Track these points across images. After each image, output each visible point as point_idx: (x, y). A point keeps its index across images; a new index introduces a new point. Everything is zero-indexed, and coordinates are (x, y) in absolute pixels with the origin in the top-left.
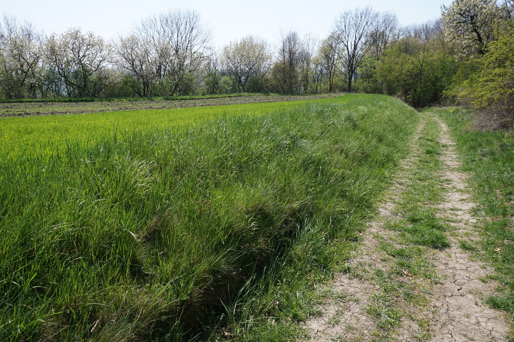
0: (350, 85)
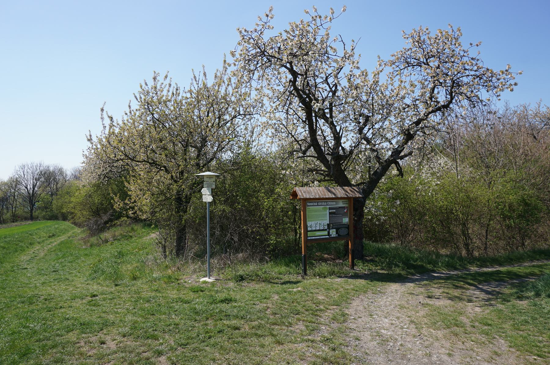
0: (31, 215)
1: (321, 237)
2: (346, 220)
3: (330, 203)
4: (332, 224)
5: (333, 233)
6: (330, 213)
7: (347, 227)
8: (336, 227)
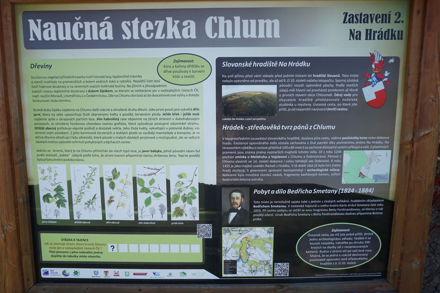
1: (149, 274)
2: (368, 167)
3: (227, 28)
4: (248, 188)
5: (251, 250)
6: (227, 109)
7: (375, 214)
8: (281, 210)
